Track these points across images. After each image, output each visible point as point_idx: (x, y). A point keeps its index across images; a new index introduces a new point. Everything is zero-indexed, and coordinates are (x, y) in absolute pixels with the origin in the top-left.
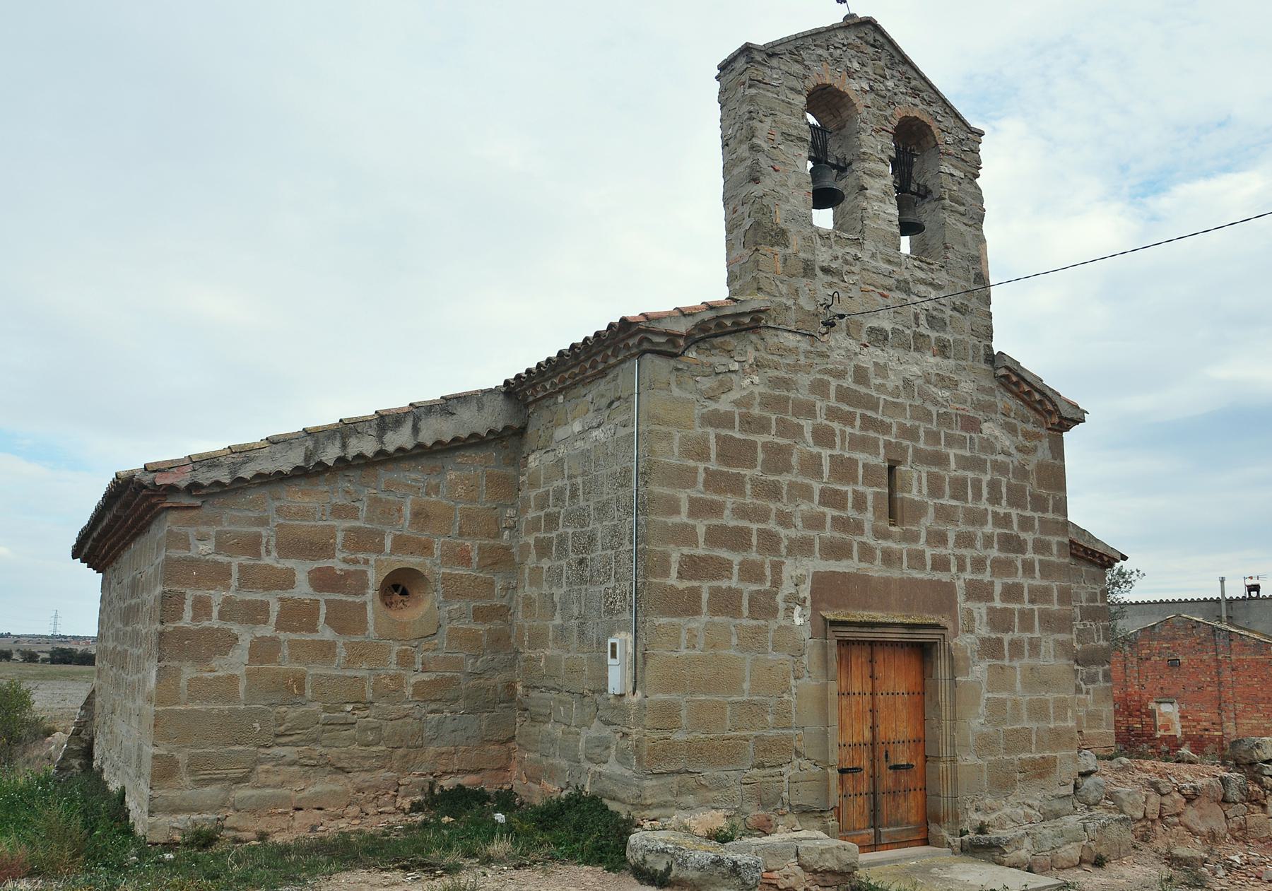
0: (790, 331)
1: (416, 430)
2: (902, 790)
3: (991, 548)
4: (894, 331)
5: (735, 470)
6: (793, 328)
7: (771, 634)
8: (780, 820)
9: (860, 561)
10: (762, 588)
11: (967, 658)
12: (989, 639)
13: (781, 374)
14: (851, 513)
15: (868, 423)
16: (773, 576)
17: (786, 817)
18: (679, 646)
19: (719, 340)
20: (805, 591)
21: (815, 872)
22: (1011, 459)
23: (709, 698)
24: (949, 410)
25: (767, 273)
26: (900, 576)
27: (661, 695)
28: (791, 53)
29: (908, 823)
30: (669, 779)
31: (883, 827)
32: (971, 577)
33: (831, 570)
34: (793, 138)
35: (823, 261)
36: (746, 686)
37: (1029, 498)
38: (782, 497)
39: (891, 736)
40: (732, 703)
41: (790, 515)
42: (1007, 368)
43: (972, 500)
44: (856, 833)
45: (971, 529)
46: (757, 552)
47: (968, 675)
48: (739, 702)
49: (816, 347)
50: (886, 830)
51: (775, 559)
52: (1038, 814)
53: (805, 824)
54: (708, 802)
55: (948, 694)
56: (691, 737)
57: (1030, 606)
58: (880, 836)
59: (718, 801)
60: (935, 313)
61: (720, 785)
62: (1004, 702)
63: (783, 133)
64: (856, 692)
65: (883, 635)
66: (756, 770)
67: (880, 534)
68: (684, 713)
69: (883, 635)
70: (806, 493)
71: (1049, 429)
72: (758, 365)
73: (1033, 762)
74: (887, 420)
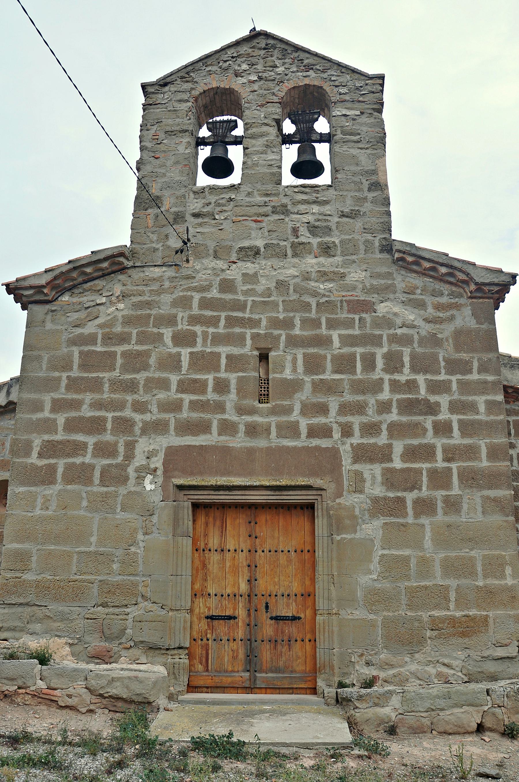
0: (155, 266)
1: (8, 393)
2: (286, 638)
3: (388, 413)
4: (266, 246)
5: (94, 375)
6: (159, 263)
7: (120, 499)
8: (124, 653)
9: (219, 434)
10: (114, 462)
12: (385, 498)
13: (146, 298)
14: (211, 395)
15: (231, 322)
16: (126, 452)
17: (131, 651)
18: (34, 508)
19: (89, 284)
20: (157, 462)
21: (101, 695)
22: (417, 330)
23: (57, 548)
24: (332, 298)
25: (138, 229)
26: (267, 445)
27: (15, 544)
28: (182, 78)
30: (20, 609)
31: (261, 671)
32: (359, 442)
33: (186, 444)
34: (175, 132)
35: (193, 209)
36: (94, 539)
37: (443, 364)
38: (138, 391)
39: (271, 588)
40: (79, 553)
42: (399, 251)
43: (362, 373)
44: (226, 674)
45: (360, 398)
46: (111, 434)
47: (355, 532)
48: (86, 552)
49: (182, 273)
50: (264, 675)
51: (129, 438)
52: (460, 674)
53: (150, 659)
54: (52, 630)
55: (325, 550)
56: (39, 578)
57: (446, 465)
58: (255, 680)
59: (60, 630)
60: (317, 224)
61: (63, 618)
62: (406, 560)
63: (166, 132)
65: (244, 497)
66: (100, 608)
67: (241, 411)
68: (34, 559)
69: (244, 497)
70: (164, 384)
71: (471, 298)
72: (124, 296)
73: (453, 621)
74: (256, 317)
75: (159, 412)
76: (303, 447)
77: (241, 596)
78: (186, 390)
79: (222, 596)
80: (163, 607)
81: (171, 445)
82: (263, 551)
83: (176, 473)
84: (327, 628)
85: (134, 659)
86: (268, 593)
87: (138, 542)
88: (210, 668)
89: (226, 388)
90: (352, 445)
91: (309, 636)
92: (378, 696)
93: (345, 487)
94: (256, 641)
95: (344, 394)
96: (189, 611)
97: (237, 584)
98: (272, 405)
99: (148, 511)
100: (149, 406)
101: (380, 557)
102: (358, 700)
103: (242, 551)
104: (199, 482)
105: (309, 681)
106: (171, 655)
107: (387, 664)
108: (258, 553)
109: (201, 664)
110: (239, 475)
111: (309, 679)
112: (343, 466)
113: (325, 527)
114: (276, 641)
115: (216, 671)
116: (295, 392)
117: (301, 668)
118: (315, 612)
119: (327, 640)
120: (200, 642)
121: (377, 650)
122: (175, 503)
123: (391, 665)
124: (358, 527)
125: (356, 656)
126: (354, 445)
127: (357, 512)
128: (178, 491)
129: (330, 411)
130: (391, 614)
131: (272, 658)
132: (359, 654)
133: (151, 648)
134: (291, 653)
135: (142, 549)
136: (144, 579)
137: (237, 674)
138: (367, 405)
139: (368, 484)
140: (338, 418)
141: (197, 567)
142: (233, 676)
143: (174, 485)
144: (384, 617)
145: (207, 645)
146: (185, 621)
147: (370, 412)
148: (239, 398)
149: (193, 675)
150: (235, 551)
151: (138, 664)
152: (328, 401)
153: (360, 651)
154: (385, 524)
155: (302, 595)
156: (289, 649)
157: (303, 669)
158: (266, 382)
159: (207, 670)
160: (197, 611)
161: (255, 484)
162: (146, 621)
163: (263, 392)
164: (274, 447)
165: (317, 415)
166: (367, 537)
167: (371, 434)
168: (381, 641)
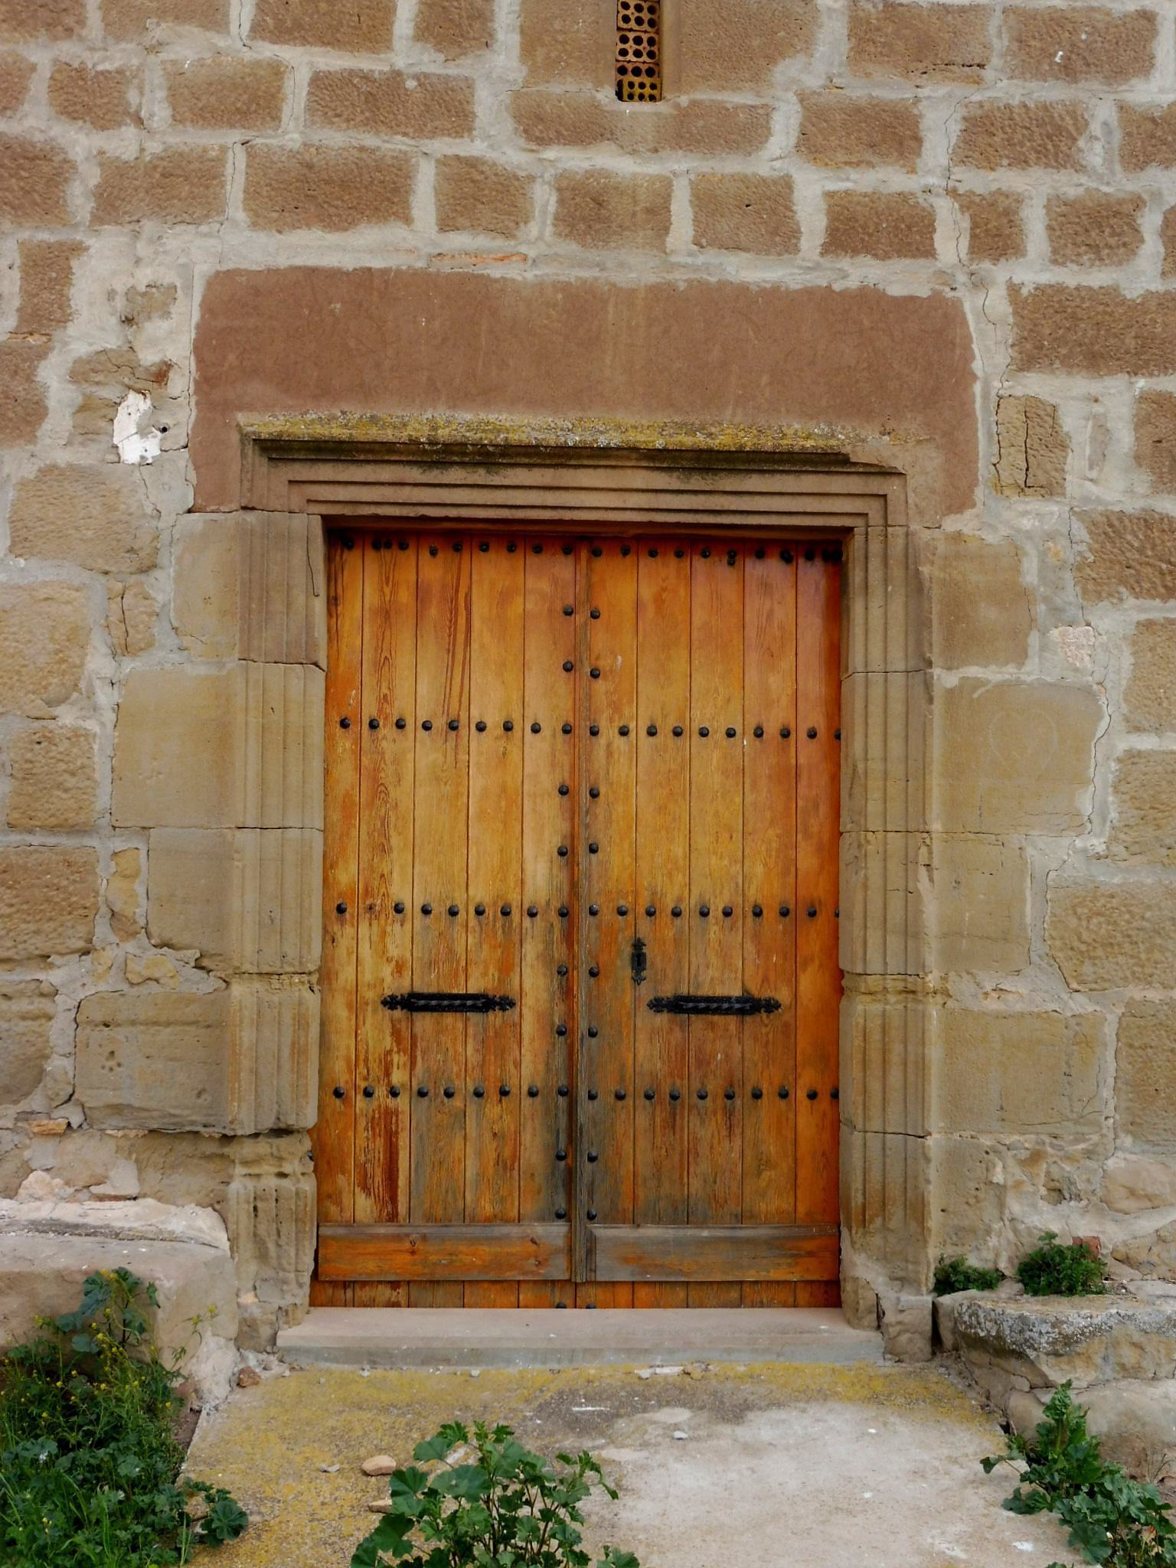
2: (715, 1086)
8: (41, 1153)
9: (446, 225)
11: (1024, 595)
26: (652, 279)
29: (741, 1218)
31: (615, 1217)
32: (1047, 277)
33: (298, 262)
41: (117, 80)
45: (1053, 92)
47: (1020, 656)
50: (625, 1232)
51: (45, 236)
53: (153, 1177)
55: (896, 727)
58: (590, 1252)
64: (494, 721)
65: (551, 499)
69: (551, 499)
75: (177, 119)
76: (809, 292)
77: (532, 915)
78: (298, 25)
79: (453, 912)
80: (205, 963)
81: (230, 266)
82: (624, 732)
83: (256, 388)
84: (897, 1049)
85: (82, 1180)
86: (643, 904)
87: (90, 685)
88: (402, 1209)
89: (477, 25)
90: (1013, 290)
91: (807, 1079)
92: (1137, 1337)
93: (984, 470)
94: (592, 1097)
95: (988, 74)
96: (314, 978)
97: (515, 867)
98: (677, 106)
99: (131, 550)
100: (132, 96)
101: (1119, 760)
102: (1057, 1354)
103: (536, 729)
104: (352, 428)
105: (810, 1254)
106: (245, 1163)
107: (1132, 1193)
108: (602, 740)
109: (366, 1188)
110: (533, 403)
111: (809, 1246)
112: (975, 377)
113: (896, 633)
114: (674, 1097)
115: (429, 1218)
116: (774, 53)
117: (774, 1203)
118: (839, 983)
119: (895, 1096)
120: (361, 1102)
121: (1095, 1138)
122: (251, 517)
123: (1148, 1197)
124: (1034, 639)
125: (1011, 1162)
126: (1025, 292)
127: (1030, 573)
128: (262, 465)
129: (926, 145)
130: (1154, 995)
131: (658, 1166)
132: (1024, 1155)
133: (151, 1131)
134: (737, 1142)
135: (110, 717)
136: (118, 844)
137: (514, 1230)
138: (1081, 125)
139: (1076, 462)
140: (959, 172)
141: (347, 795)
142: (498, 1239)
143: (244, 437)
144: (1127, 1005)
145: (390, 1114)
146: (301, 1022)
147: (1095, 153)
148: (533, 71)
149: (333, 1238)
150: (508, 727)
151: (101, 1198)
152: (917, 100)
153: (1028, 1141)
154: (1148, 626)
155: (785, 913)
156: (730, 1128)
157: (785, 1206)
158: (645, 15)
159: (393, 1217)
160: (346, 975)
161: (603, 441)
162: (133, 1023)
163: (631, 57)
164: (682, 286)
165: (868, 156)
166: (1071, 678)
167: (1095, 248)
168: (1112, 1105)
